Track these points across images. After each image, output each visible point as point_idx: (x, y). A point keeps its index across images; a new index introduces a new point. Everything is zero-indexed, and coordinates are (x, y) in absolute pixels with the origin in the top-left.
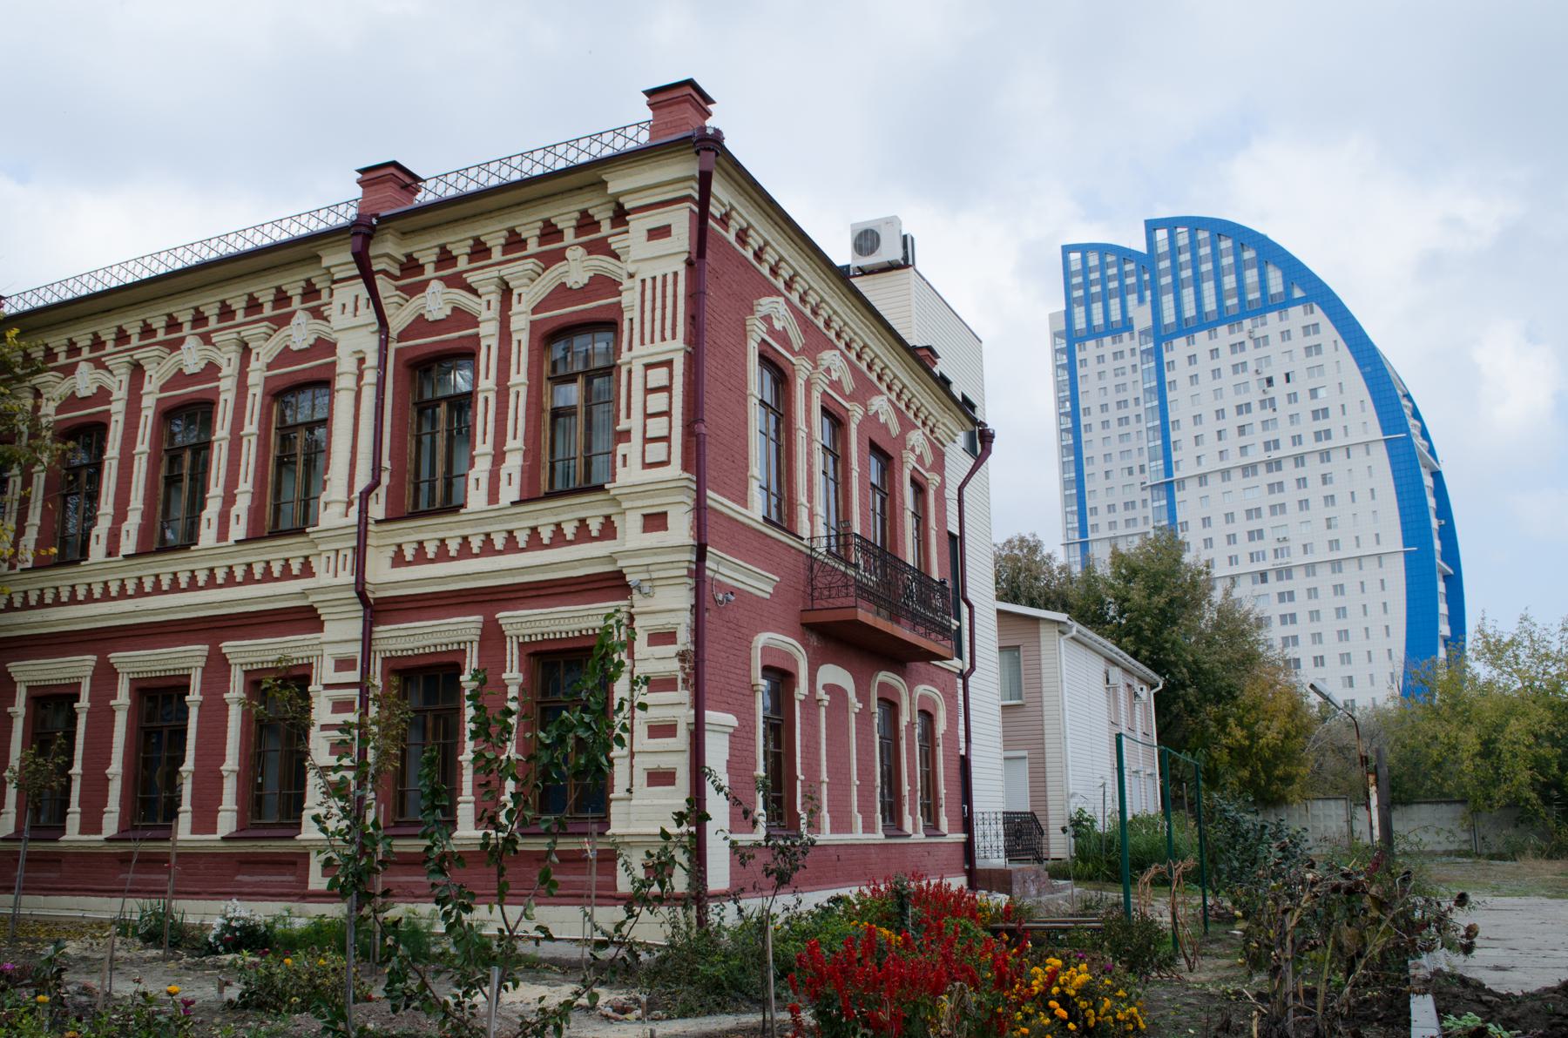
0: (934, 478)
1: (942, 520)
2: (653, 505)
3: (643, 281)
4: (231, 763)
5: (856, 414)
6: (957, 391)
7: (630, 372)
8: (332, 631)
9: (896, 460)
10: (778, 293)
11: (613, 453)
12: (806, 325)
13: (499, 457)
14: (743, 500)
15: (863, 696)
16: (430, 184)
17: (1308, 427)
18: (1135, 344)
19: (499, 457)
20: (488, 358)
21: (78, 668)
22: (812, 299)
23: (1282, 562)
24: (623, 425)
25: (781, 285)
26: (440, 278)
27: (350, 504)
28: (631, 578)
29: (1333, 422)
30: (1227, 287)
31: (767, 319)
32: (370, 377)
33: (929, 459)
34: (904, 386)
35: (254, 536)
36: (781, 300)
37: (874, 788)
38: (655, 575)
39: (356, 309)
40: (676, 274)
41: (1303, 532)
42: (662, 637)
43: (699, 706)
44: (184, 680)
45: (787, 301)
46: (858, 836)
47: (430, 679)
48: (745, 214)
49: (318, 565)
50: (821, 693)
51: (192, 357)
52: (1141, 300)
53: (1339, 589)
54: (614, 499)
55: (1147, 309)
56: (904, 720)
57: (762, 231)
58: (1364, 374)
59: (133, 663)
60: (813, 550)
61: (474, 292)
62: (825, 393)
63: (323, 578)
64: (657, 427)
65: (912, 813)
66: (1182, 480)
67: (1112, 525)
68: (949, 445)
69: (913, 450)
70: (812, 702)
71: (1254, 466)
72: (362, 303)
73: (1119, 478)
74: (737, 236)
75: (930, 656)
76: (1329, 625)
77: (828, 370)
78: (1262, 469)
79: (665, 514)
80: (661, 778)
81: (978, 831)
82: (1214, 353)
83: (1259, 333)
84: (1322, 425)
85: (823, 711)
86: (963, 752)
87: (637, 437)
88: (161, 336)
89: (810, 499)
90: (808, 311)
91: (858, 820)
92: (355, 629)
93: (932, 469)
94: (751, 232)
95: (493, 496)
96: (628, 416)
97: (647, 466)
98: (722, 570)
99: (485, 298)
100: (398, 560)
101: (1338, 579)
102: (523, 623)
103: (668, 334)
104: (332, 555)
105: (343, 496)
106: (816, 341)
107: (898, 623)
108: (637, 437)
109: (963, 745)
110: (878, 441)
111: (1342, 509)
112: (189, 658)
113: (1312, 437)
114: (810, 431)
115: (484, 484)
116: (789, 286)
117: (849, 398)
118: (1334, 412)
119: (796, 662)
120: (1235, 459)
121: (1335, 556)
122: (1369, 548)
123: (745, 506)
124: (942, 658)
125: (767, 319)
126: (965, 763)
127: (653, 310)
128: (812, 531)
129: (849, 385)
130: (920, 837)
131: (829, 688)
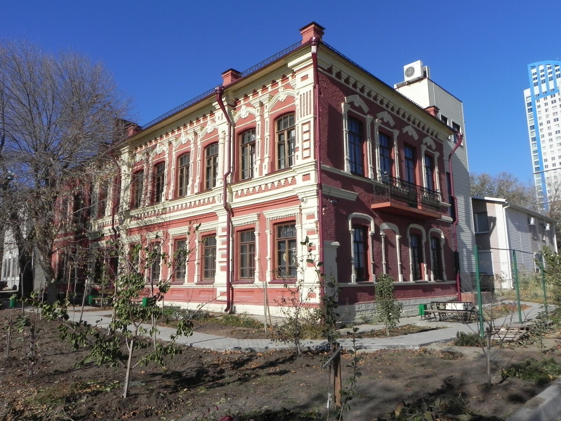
2: (305, 171)
4: (424, 249)
5: (396, 133)
13: (262, 160)
19: (262, 160)
20: (258, 130)
22: (373, 94)
28: (300, 197)
36: (358, 96)
38: (307, 195)
42: (310, 216)
47: (247, 233)
59: (174, 231)
87: (300, 149)
93: (436, 150)
95: (261, 173)
108: (300, 149)
127: (304, 105)
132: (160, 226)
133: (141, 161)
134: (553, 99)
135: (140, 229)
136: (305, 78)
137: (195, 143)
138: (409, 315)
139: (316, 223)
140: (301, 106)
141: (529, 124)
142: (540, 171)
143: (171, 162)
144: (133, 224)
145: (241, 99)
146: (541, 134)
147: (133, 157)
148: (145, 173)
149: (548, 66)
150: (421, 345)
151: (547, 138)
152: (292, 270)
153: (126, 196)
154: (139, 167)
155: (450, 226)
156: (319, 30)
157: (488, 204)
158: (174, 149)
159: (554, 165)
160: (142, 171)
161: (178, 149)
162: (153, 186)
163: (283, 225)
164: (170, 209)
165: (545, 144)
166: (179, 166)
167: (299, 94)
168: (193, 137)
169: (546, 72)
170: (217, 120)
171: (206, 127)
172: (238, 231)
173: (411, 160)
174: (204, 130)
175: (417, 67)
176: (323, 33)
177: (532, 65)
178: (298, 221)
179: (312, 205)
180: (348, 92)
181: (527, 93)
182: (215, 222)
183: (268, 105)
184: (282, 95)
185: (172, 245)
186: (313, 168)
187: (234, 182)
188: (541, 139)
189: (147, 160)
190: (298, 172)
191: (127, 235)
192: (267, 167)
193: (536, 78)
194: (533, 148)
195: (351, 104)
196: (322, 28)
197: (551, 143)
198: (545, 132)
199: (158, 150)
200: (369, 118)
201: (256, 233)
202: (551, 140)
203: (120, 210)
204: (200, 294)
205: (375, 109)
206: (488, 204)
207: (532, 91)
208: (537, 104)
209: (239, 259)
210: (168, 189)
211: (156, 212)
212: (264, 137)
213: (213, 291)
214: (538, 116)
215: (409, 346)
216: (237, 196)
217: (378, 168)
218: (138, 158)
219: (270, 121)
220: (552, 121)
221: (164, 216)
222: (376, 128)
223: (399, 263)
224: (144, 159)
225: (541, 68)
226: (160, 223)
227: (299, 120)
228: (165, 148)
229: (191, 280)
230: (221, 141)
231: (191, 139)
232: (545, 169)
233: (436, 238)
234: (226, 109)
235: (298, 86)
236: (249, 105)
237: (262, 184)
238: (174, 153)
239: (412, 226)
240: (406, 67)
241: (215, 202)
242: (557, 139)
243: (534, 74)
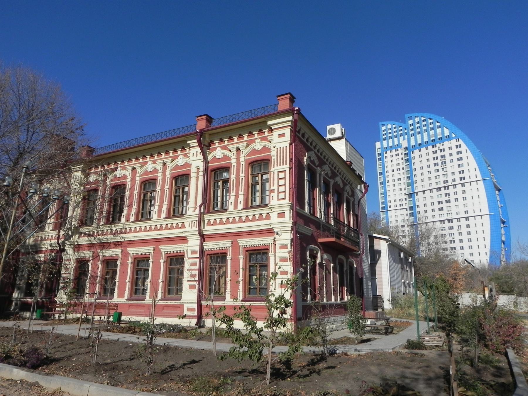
0: (352, 199)
2: (281, 210)
5: (332, 182)
8: (190, 243)
11: (269, 196)
12: (319, 158)
13: (237, 196)
17: (457, 176)
18: (402, 151)
19: (237, 196)
20: (233, 170)
21: (116, 252)
23: (450, 217)
24: (272, 188)
26: (220, 147)
27: (195, 208)
28: (275, 230)
29: (465, 175)
30: (431, 134)
32: (201, 173)
35: (168, 217)
39: (197, 155)
41: (456, 209)
42: (283, 247)
44: (148, 256)
47: (220, 257)
49: (186, 225)
51: (150, 167)
52: (404, 139)
53: (468, 226)
54: (270, 208)
55: (406, 141)
56: (345, 269)
58: (475, 159)
59: (133, 251)
61: (230, 151)
63: (188, 228)
64: (282, 189)
66: (417, 193)
67: (396, 206)
71: (440, 188)
72: (198, 153)
73: (397, 192)
76: (465, 237)
78: (443, 189)
82: (428, 154)
83: (442, 147)
84: (462, 175)
87: (276, 191)
90: (319, 154)
92: (198, 242)
93: (351, 196)
95: (236, 207)
96: (273, 186)
101: (467, 223)
103: (285, 163)
105: (193, 206)
111: (469, 201)
112: (148, 250)
113: (459, 179)
117: (330, 178)
118: (466, 171)
120: (434, 186)
121: (467, 215)
122: (478, 213)
132: (116, 244)
133: (97, 181)
134: (397, 152)
135: (91, 246)
137: (164, 173)
138: (338, 329)
139: (289, 252)
140: (277, 157)
141: (379, 170)
142: (385, 210)
143: (133, 186)
144: (84, 240)
145: (216, 142)
146: (387, 179)
147: (87, 175)
148: (100, 193)
149: (394, 126)
150: (393, 349)
151: (391, 183)
152: (179, 290)
153: (74, 213)
154: (93, 186)
155: (55, 229)
156: (292, 100)
157: (375, 240)
158: (138, 175)
160: (96, 190)
161: (142, 175)
162: (110, 206)
163: (255, 252)
165: (390, 188)
166: (142, 191)
167: (276, 147)
168: (162, 167)
169: (392, 130)
170: (191, 155)
172: (208, 255)
173: (338, 204)
174: (174, 162)
175: (338, 128)
176: (294, 102)
177: (383, 123)
178: (271, 249)
179: (286, 237)
180: (308, 149)
181: (378, 145)
182: (185, 245)
183: (245, 152)
184: (258, 145)
185: (131, 263)
186: (289, 209)
187: (206, 211)
188: (387, 184)
189: (104, 181)
191: (74, 251)
192: (242, 203)
193: (385, 134)
194: (381, 191)
195: (309, 158)
196: (294, 98)
197: (394, 188)
198: (390, 178)
199: (119, 173)
201: (229, 257)
202: (394, 185)
203: (68, 226)
204: (163, 309)
205: (322, 163)
206: (375, 240)
207: (382, 144)
208: (385, 155)
209: (208, 278)
210: (130, 210)
211: (114, 232)
212: (239, 176)
213: (181, 307)
214: (386, 165)
215: (386, 349)
216: (209, 224)
217: (322, 210)
218: (92, 178)
219: (245, 164)
220: (395, 170)
221: (123, 235)
222: (322, 178)
223: (332, 287)
224: (100, 179)
225: (389, 126)
226: (118, 242)
227: (275, 169)
228: (128, 173)
229: (121, 295)
230: (193, 175)
231: (158, 168)
232: (389, 209)
233: (351, 267)
235: (275, 141)
236: (225, 148)
237: (235, 216)
238: (137, 179)
240: (329, 127)
242: (438, 197)
243: (383, 131)
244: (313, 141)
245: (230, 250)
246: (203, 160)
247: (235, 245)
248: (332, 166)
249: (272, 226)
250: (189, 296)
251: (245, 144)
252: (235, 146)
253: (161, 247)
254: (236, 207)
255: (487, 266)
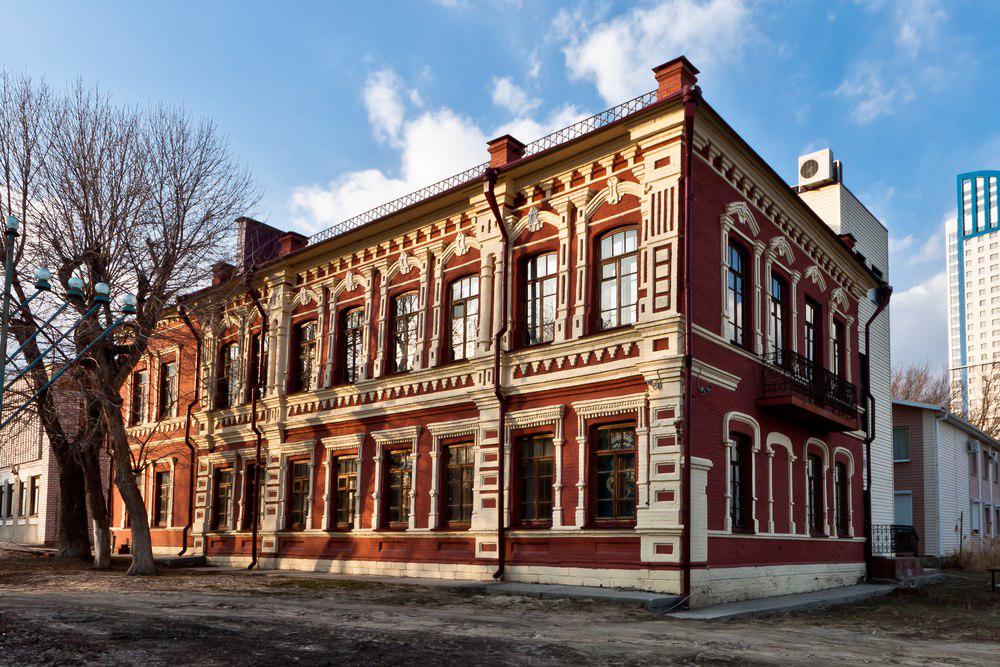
1: (855, 345)
2: (659, 334)
3: (653, 195)
6: (868, 264)
7: (646, 253)
8: (484, 416)
9: (824, 309)
10: (743, 199)
14: (718, 330)
15: (797, 450)
16: (529, 148)
24: (643, 286)
25: (745, 195)
27: (491, 343)
31: (735, 216)
32: (498, 268)
33: (847, 307)
34: (830, 260)
36: (744, 204)
37: (725, 499)
39: (490, 228)
40: (672, 189)
43: (687, 453)
45: (749, 204)
46: (793, 535)
48: (719, 147)
49: (475, 378)
50: (770, 449)
57: (731, 159)
60: (764, 362)
62: (774, 264)
63: (478, 386)
65: (830, 523)
68: (862, 298)
69: (836, 300)
70: (763, 455)
72: (493, 224)
74: (714, 161)
75: (841, 428)
77: (777, 249)
79: (667, 339)
80: (665, 496)
81: (874, 537)
85: (771, 460)
86: (865, 489)
87: (650, 294)
88: (388, 253)
89: (764, 330)
91: (794, 526)
92: (497, 414)
94: (724, 159)
95: (568, 334)
96: (645, 281)
97: (655, 310)
98: (703, 372)
99: (561, 215)
100: (517, 375)
102: (585, 408)
103: (668, 227)
104: (482, 372)
106: (768, 232)
107: (823, 407)
109: (865, 484)
110: (810, 294)
114: (766, 287)
115: (563, 329)
116: (751, 194)
117: (791, 267)
119: (753, 430)
123: (719, 334)
124: (850, 430)
125: (735, 216)
126: (866, 496)
128: (764, 350)
129: (791, 259)
130: (835, 538)
131: (774, 446)
136: (661, 163)
139: (677, 425)
152: (629, 507)
158: (383, 283)
159: (983, 357)
164: (175, 426)
170: (477, 231)
171: (452, 245)
178: (641, 419)
182: (474, 420)
183: (583, 209)
190: (643, 335)
200: (760, 247)
231: (420, 266)
234: (501, 209)
239: (811, 441)
241: (473, 384)
244: (745, 176)
245: (559, 430)
246: (501, 238)
247: (568, 414)
248: (799, 241)
249: (641, 370)
250: (484, 525)
251: (586, 191)
252: (565, 199)
253: (431, 426)
254: (568, 334)
255: (910, 236)
